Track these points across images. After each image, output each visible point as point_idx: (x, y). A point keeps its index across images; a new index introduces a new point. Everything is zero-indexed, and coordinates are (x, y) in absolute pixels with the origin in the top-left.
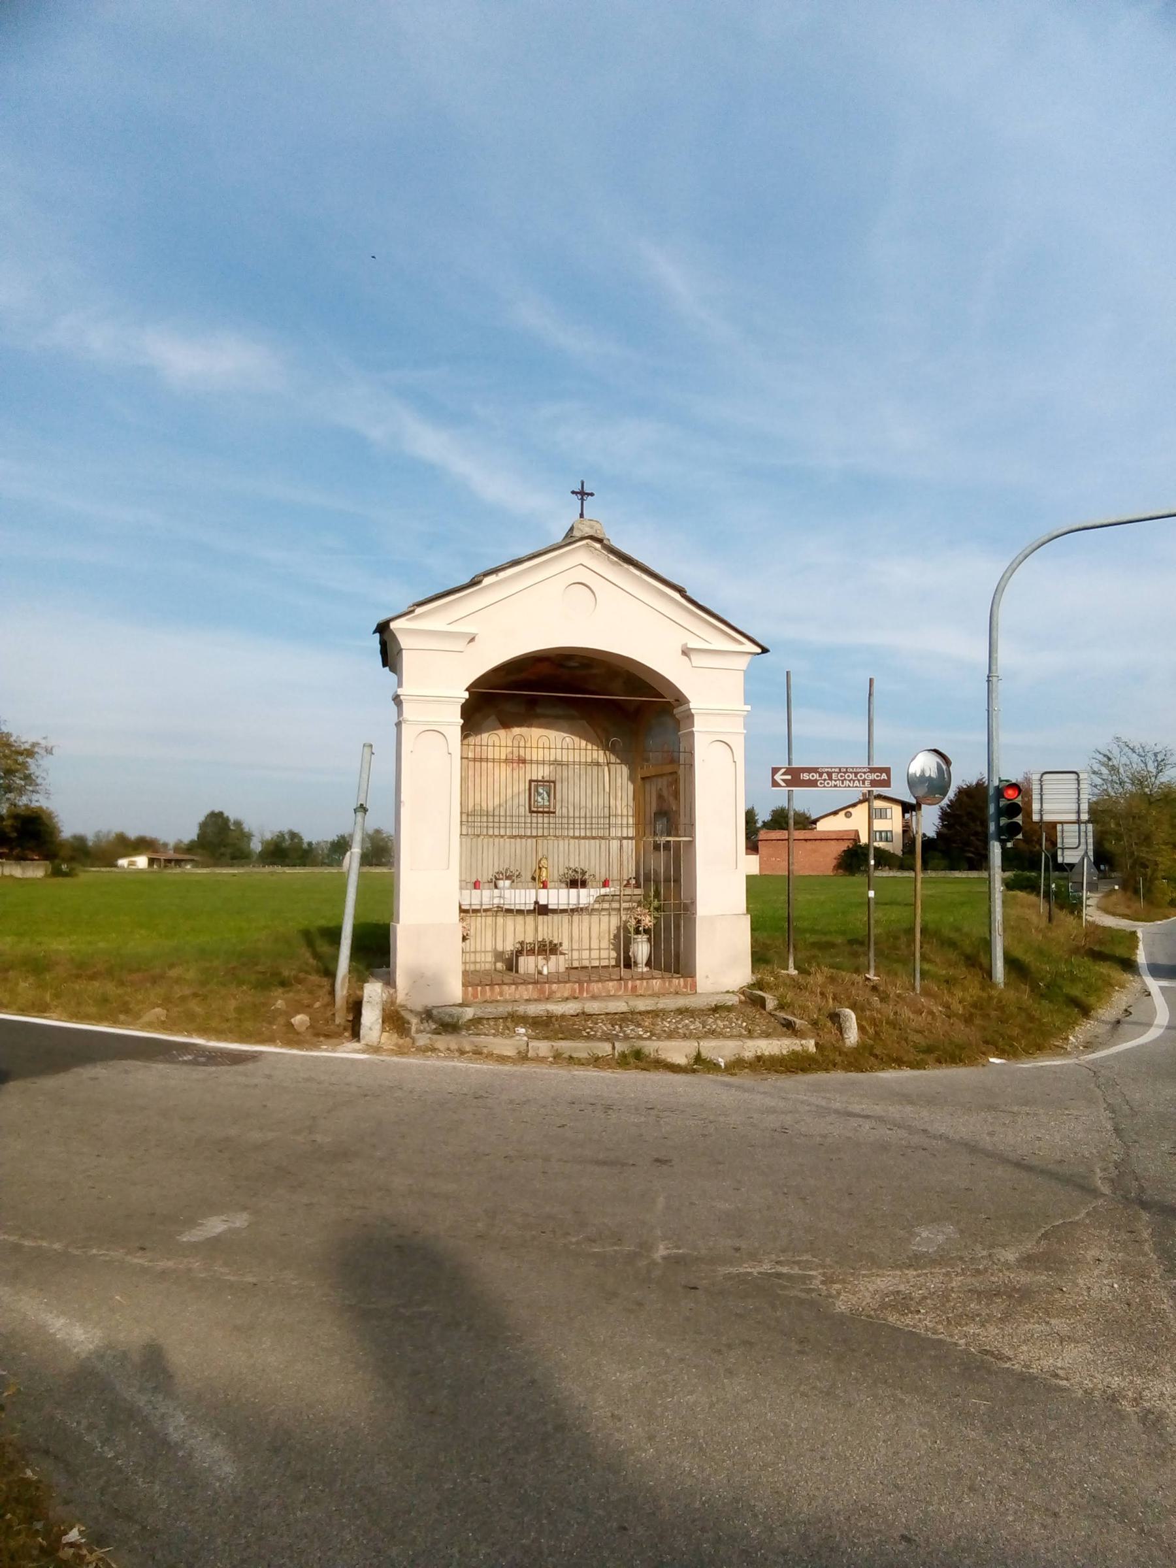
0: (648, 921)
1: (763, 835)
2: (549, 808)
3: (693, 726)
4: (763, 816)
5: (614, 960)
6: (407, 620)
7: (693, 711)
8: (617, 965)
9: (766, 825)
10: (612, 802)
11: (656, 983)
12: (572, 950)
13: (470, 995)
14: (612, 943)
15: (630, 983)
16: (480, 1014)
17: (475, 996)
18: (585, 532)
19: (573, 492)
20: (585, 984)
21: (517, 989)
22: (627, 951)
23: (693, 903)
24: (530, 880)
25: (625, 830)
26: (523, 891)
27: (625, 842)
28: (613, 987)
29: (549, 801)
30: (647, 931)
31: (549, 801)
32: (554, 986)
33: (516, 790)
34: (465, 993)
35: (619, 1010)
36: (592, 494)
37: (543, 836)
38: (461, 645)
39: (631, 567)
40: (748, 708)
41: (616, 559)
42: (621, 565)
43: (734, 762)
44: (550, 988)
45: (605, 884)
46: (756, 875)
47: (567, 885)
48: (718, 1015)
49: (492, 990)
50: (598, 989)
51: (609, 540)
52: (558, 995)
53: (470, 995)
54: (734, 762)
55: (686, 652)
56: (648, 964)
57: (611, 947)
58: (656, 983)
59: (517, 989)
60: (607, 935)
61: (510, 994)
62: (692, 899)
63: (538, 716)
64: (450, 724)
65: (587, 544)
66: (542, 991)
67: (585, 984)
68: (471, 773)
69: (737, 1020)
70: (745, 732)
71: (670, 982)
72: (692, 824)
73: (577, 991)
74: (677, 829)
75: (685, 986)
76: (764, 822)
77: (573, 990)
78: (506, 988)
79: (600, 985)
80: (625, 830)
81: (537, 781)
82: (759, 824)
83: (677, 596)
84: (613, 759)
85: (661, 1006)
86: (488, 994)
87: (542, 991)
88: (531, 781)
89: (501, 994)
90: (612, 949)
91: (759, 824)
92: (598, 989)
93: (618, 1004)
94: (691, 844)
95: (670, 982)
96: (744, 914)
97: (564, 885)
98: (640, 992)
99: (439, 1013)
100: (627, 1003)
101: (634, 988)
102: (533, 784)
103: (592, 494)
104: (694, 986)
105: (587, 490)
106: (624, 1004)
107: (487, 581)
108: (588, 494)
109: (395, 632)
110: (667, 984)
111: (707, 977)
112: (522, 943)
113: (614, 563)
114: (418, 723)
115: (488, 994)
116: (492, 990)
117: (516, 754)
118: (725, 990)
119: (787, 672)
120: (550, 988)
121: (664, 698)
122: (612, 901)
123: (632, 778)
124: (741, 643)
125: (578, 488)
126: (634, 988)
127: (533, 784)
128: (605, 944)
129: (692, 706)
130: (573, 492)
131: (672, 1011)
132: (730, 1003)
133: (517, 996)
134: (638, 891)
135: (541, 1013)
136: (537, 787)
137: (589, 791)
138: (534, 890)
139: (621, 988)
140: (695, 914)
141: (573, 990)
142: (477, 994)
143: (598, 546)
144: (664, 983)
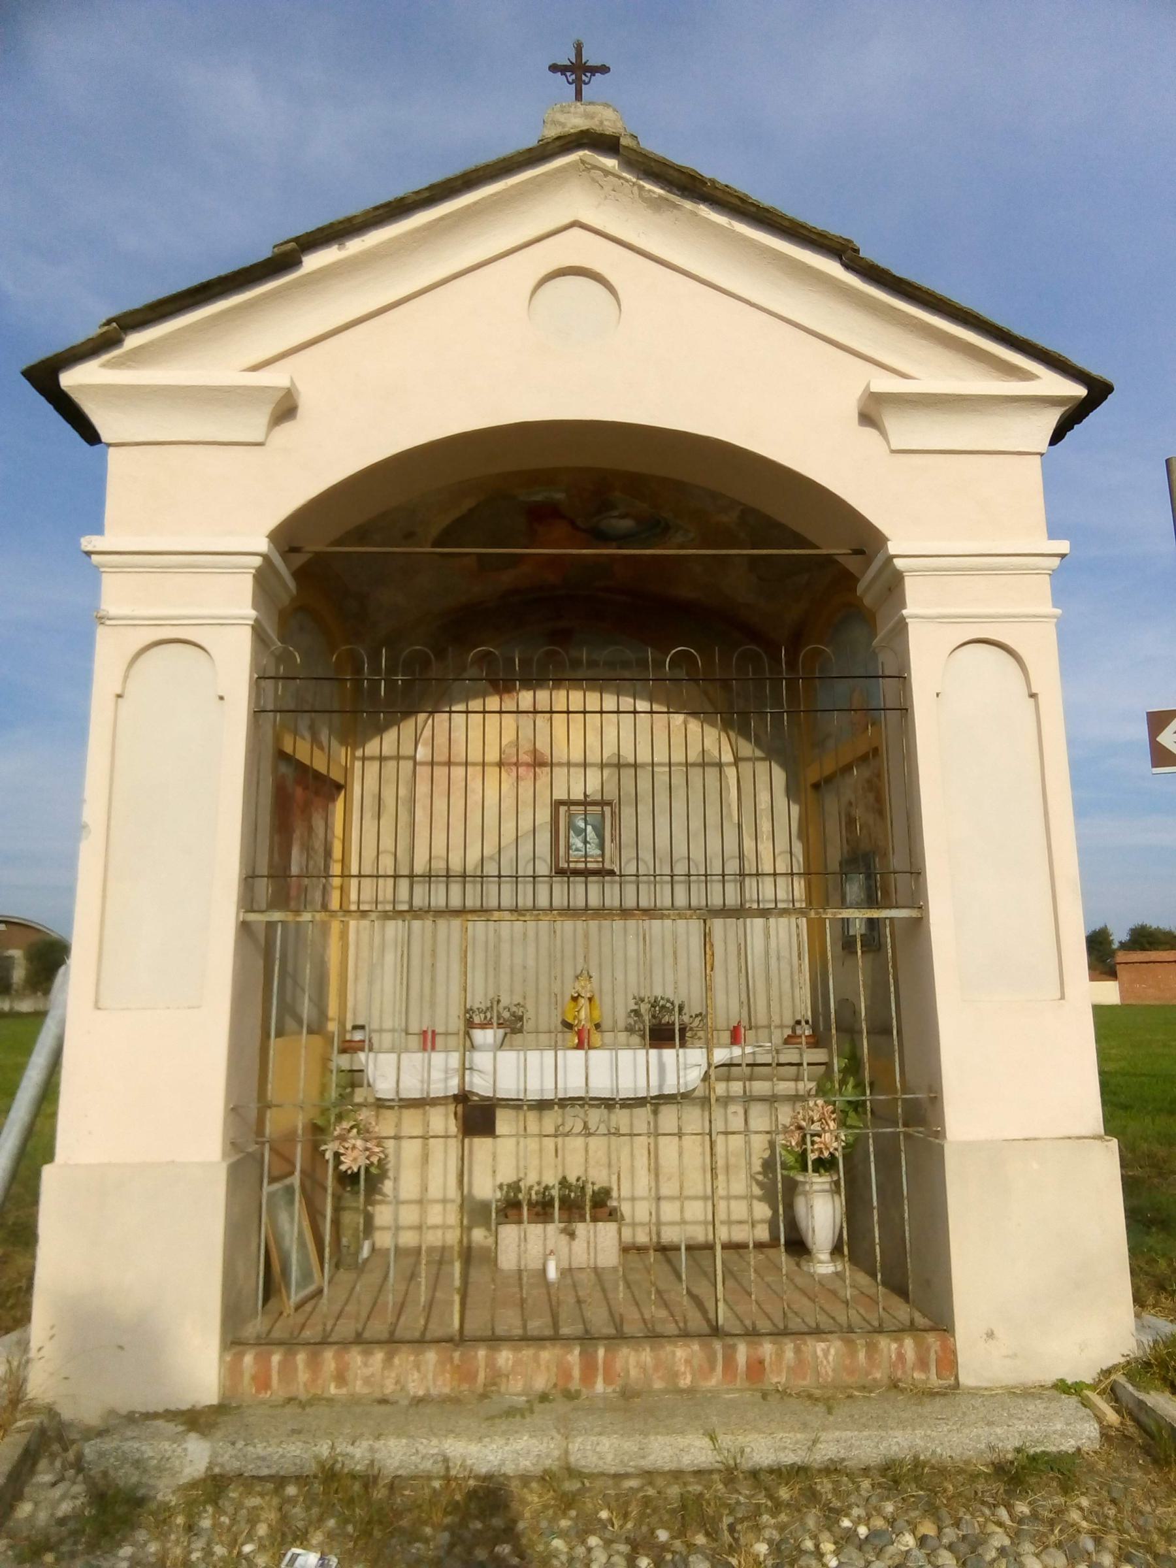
0: (831, 1141)
1: (1121, 957)
2: (603, 862)
3: (903, 605)
4: (1119, 935)
5: (766, 1226)
6: (103, 366)
7: (899, 563)
8: (774, 1243)
9: (1124, 946)
10: (748, 844)
11: (826, 1353)
12: (659, 1199)
13: (247, 1378)
14: (759, 1183)
15: (742, 1352)
16: (230, 1460)
17: (263, 1382)
18: (569, 125)
19: (554, 68)
20: (601, 1352)
21: (389, 1359)
22: (790, 1207)
23: (936, 1100)
24: (560, 1027)
25: (716, 888)
26: (549, 1055)
27: (717, 924)
28: (688, 1362)
29: (602, 846)
30: (825, 1165)
31: (602, 846)
32: (505, 1357)
33: (526, 824)
34: (232, 1372)
35: (687, 1461)
36: (604, 69)
37: (515, 910)
38: (253, 424)
39: (702, 207)
40: (1063, 546)
41: (659, 191)
42: (676, 206)
43: (1033, 696)
44: (491, 1364)
45: (735, 1038)
46: (1116, 1006)
47: (643, 1036)
48: (1022, 1508)
49: (314, 1364)
50: (643, 1368)
51: (634, 137)
52: (516, 1385)
53: (247, 1378)
54: (1033, 696)
55: (868, 418)
56: (836, 1251)
57: (757, 1191)
58: (826, 1353)
59: (389, 1359)
60: (743, 1163)
61: (367, 1381)
62: (930, 1090)
63: (576, 664)
64: (222, 622)
65: (583, 162)
66: (466, 1374)
67: (601, 1352)
68: (422, 789)
69: (1098, 1541)
70: (1058, 611)
71: (872, 1348)
72: (917, 873)
73: (576, 1373)
74: (886, 893)
75: (923, 1364)
76: (1121, 943)
77: (565, 1372)
78: (355, 1357)
79: (647, 1355)
80: (716, 888)
81: (569, 803)
82: (1115, 946)
83: (832, 267)
84: (747, 748)
85: (827, 1450)
86: (303, 1376)
87: (466, 1374)
88: (557, 804)
89: (341, 1378)
90: (760, 1199)
91: (1115, 946)
92: (643, 1368)
93: (682, 1441)
94: (918, 927)
95: (872, 1348)
96: (1099, 1138)
97: (636, 1039)
98: (776, 1379)
99: (102, 1455)
100: (713, 1439)
101: (756, 1368)
102: (563, 809)
103: (604, 69)
104: (949, 1361)
105: (591, 57)
106: (706, 1442)
107: (313, 262)
108: (579, 53)
109: (74, 396)
110: (862, 1355)
111: (991, 1335)
112: (515, 1187)
113: (657, 205)
114: (133, 622)
115: (303, 1376)
116: (314, 1364)
117: (525, 746)
118: (1050, 1378)
119: (1167, 461)
120: (491, 1364)
121: (818, 548)
122: (751, 1079)
123: (792, 791)
124: (1027, 376)
125: (566, 57)
126: (756, 1368)
127: (563, 809)
128: (739, 1184)
129: (893, 548)
130: (554, 68)
131: (866, 1471)
132: (1069, 1446)
133: (389, 1387)
134: (819, 1055)
135: (428, 1465)
136: (570, 816)
137: (696, 824)
138: (552, 1053)
139: (712, 1368)
140: (941, 1134)
141: (565, 1372)
142: (268, 1378)
143: (611, 163)
144: (853, 1354)
